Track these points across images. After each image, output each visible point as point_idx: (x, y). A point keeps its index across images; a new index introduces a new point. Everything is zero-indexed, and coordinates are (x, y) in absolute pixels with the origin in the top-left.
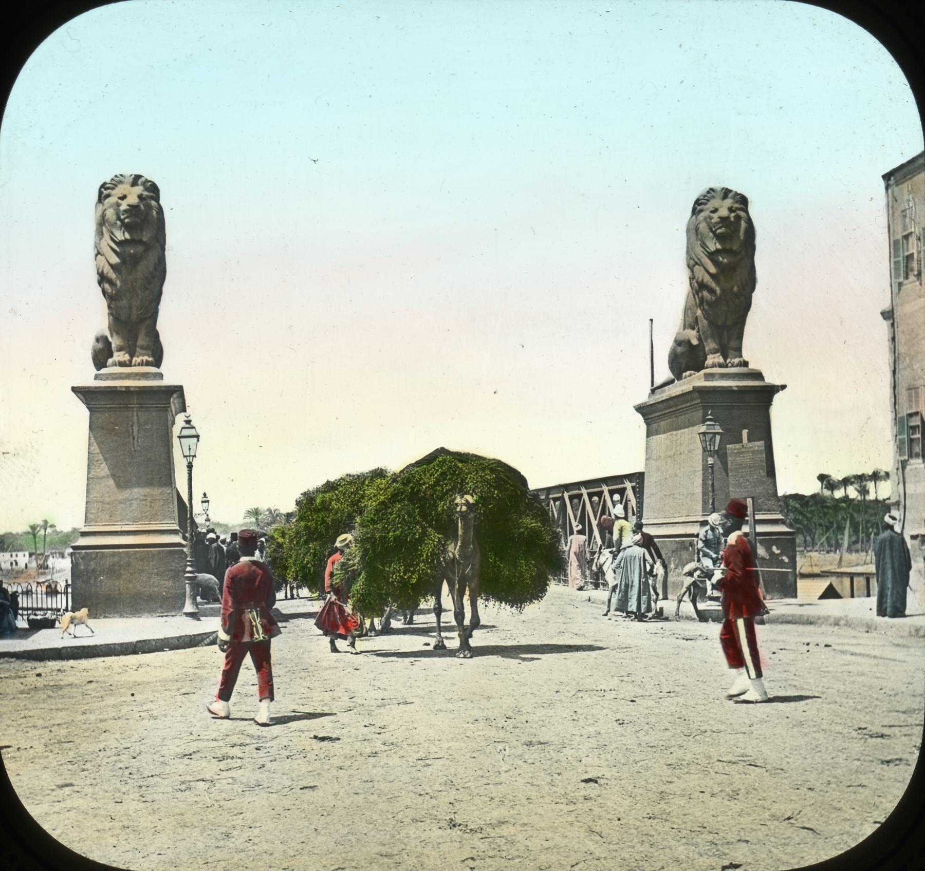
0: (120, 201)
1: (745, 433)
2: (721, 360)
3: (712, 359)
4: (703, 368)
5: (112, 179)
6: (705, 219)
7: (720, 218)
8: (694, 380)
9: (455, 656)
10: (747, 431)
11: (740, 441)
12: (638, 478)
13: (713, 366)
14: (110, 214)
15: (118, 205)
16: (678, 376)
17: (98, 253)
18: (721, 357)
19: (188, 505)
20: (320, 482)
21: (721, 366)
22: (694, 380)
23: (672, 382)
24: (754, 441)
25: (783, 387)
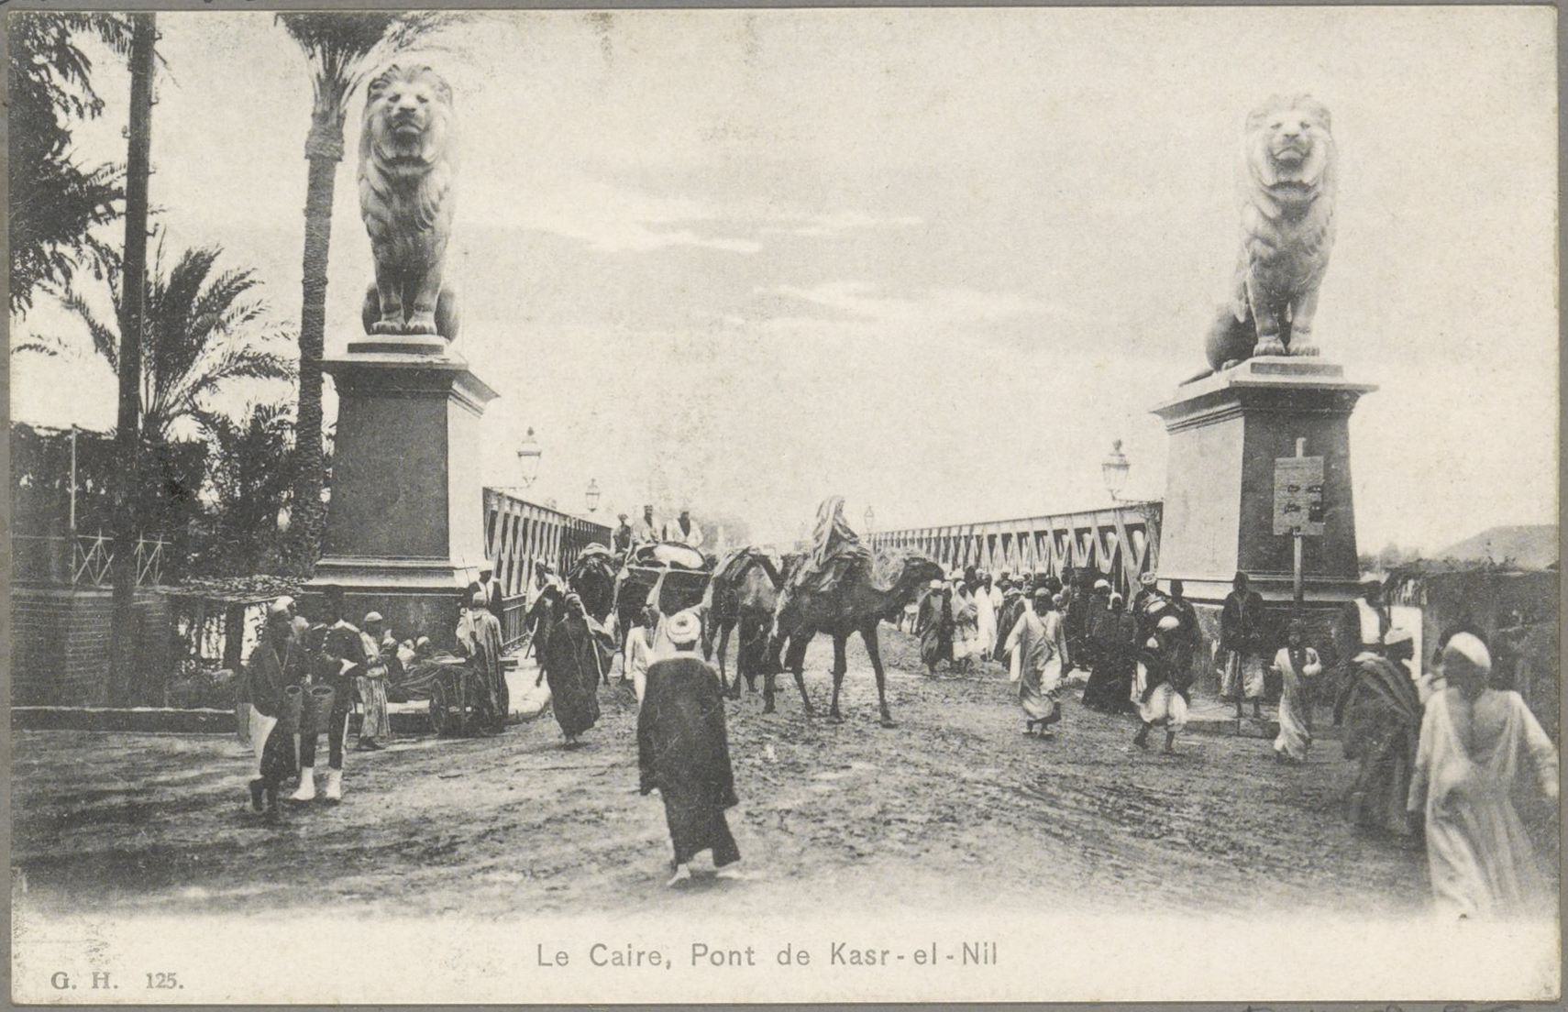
0: (391, 104)
1: (1300, 442)
2: (1280, 346)
3: (1262, 344)
4: (1251, 356)
5: (384, 74)
6: (382, 111)
7: (401, 109)
8: (1242, 373)
9: (84, 430)
10: (1304, 439)
11: (1293, 454)
12: (1157, 507)
13: (1265, 353)
14: (378, 124)
15: (389, 109)
16: (1218, 367)
17: (363, 177)
18: (1279, 340)
19: (720, 677)
20: (324, 409)
21: (1279, 353)
22: (1242, 373)
23: (1209, 374)
24: (1295, 451)
25: (1375, 389)
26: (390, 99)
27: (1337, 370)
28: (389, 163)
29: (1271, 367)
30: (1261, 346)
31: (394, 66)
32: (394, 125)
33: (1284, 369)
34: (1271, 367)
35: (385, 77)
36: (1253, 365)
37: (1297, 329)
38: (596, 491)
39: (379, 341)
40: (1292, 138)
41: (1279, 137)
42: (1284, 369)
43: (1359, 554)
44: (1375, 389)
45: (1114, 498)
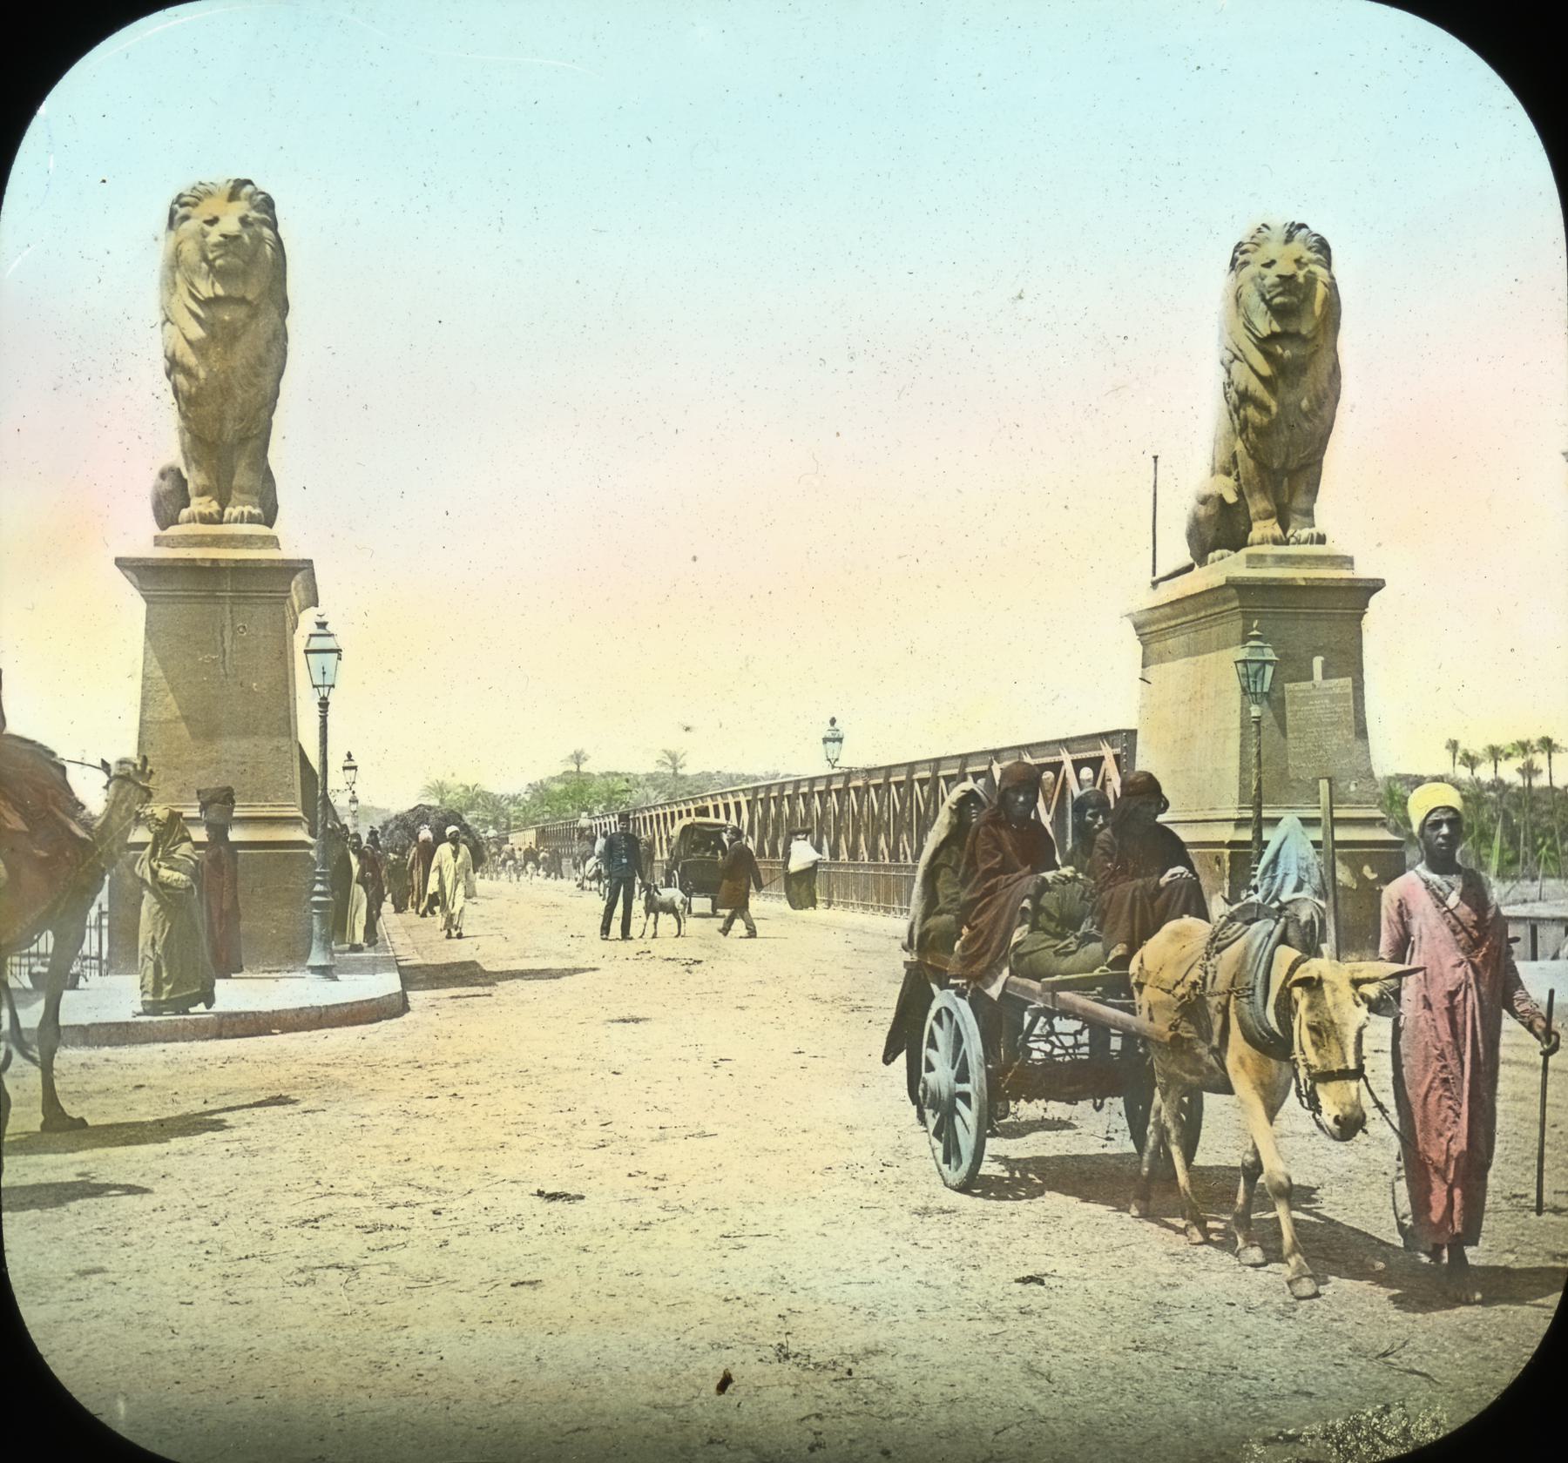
0: (207, 228)
2: (1278, 531)
8: (1228, 566)
10: (1322, 658)
11: (1310, 678)
13: (240, 519)
14: (190, 250)
15: (205, 235)
21: (1276, 542)
22: (1228, 566)
23: (1189, 568)
25: (121, 563)
26: (206, 222)
27: (1348, 561)
28: (206, 303)
29: (200, 541)
30: (1255, 535)
31: (1264, 225)
32: (211, 256)
33: (1282, 560)
34: (200, 541)
35: (1255, 240)
36: (1250, 558)
37: (1295, 512)
38: (352, 764)
40: (1286, 281)
41: (1271, 276)
42: (217, 541)
43: (204, 828)
44: (121, 563)
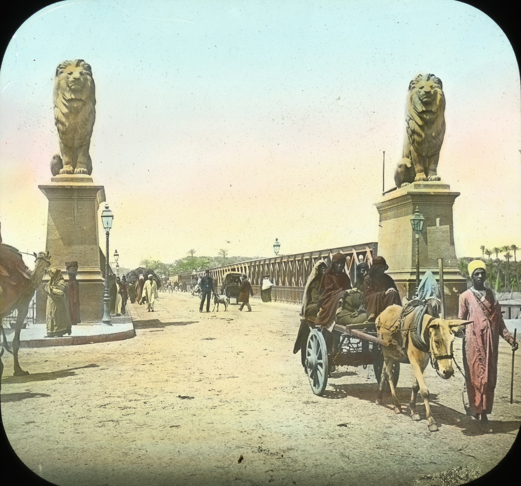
0: (69, 76)
2: (425, 177)
8: (408, 188)
10: (439, 219)
11: (435, 225)
13: (80, 173)
14: (63, 83)
15: (68, 78)
21: (424, 180)
22: (408, 188)
23: (395, 189)
25: (40, 187)
26: (69, 74)
27: (448, 186)
28: (69, 101)
29: (67, 180)
30: (417, 178)
31: (420, 75)
32: (70, 85)
33: (426, 186)
34: (67, 180)
35: (417, 80)
36: (415, 185)
37: (430, 170)
39: (84, 185)
40: (427, 93)
41: (422, 92)
42: (72, 180)
43: (68, 275)
44: (40, 187)
45: (277, 255)
